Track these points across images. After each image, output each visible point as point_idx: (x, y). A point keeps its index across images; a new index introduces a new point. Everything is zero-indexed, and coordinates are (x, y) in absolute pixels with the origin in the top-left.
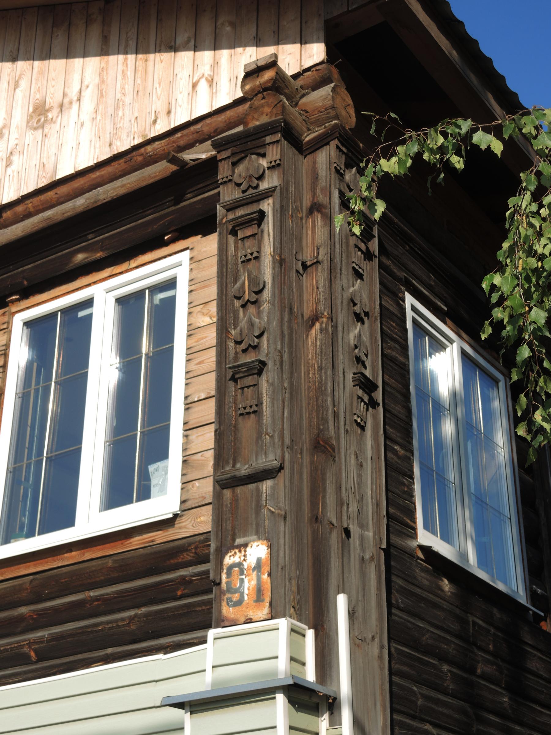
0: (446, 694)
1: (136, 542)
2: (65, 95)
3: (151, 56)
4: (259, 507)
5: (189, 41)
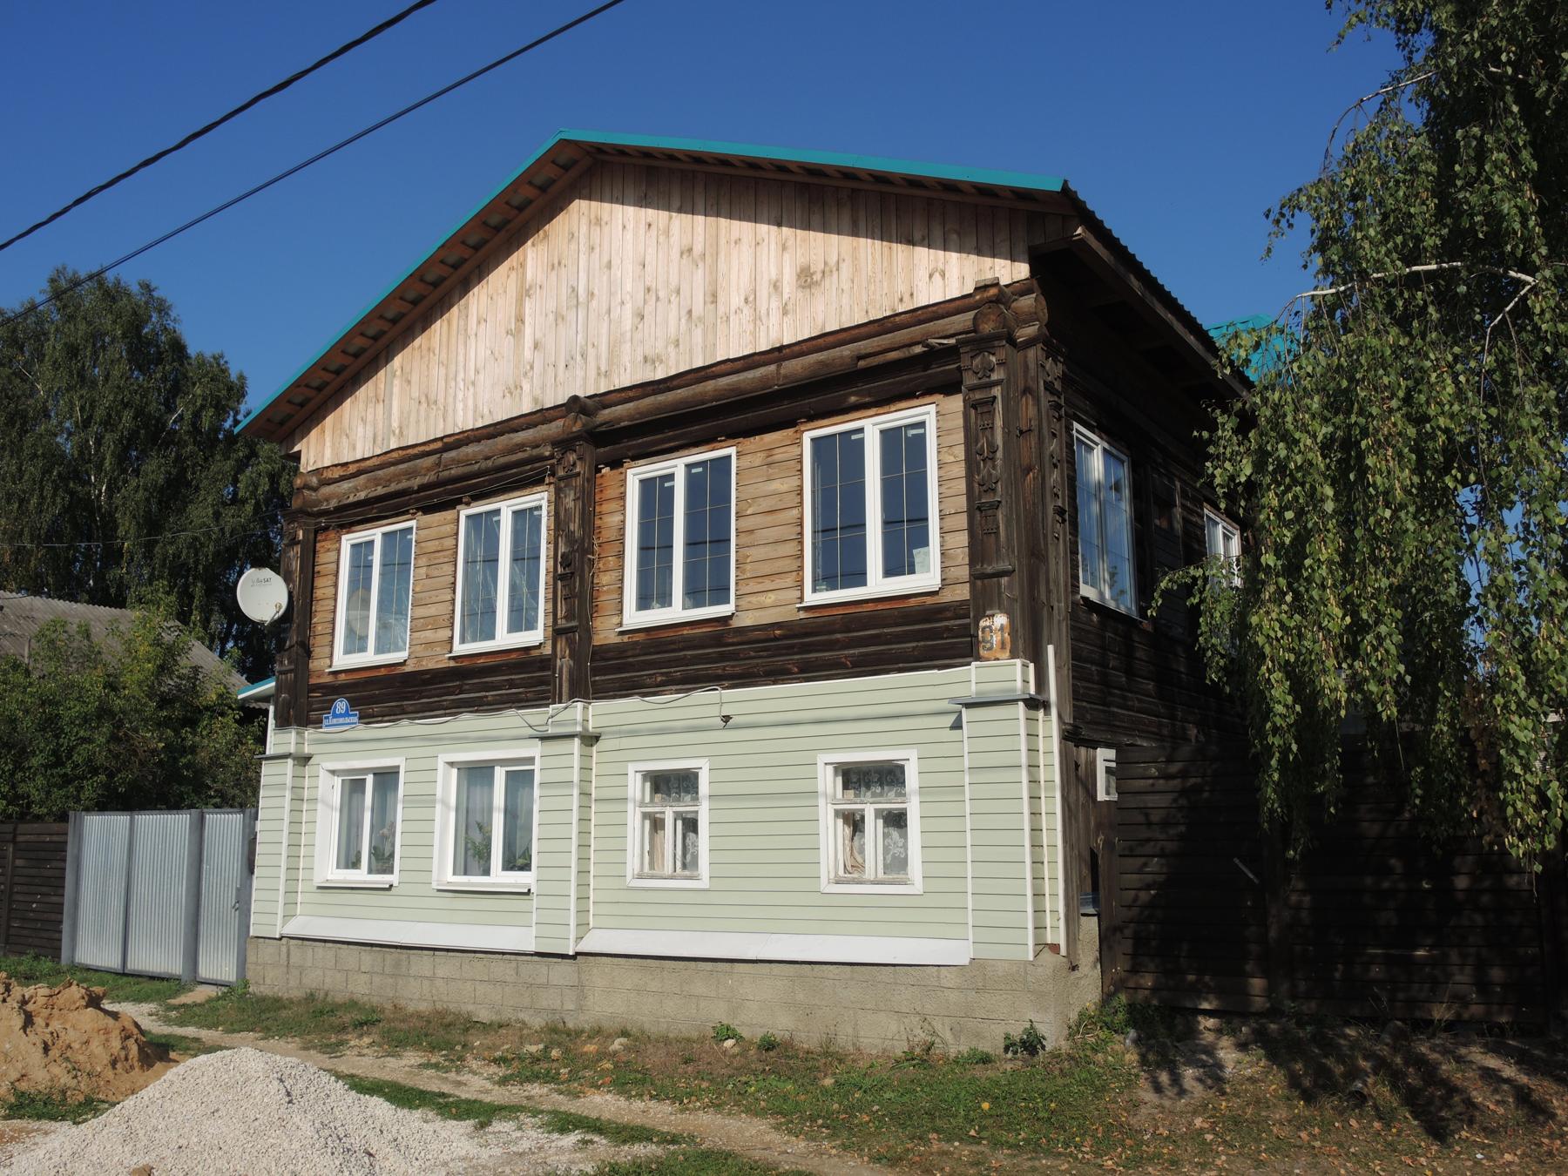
0: (1093, 683)
1: (912, 602)
2: (826, 263)
3: (894, 245)
4: (1000, 593)
5: (923, 239)
